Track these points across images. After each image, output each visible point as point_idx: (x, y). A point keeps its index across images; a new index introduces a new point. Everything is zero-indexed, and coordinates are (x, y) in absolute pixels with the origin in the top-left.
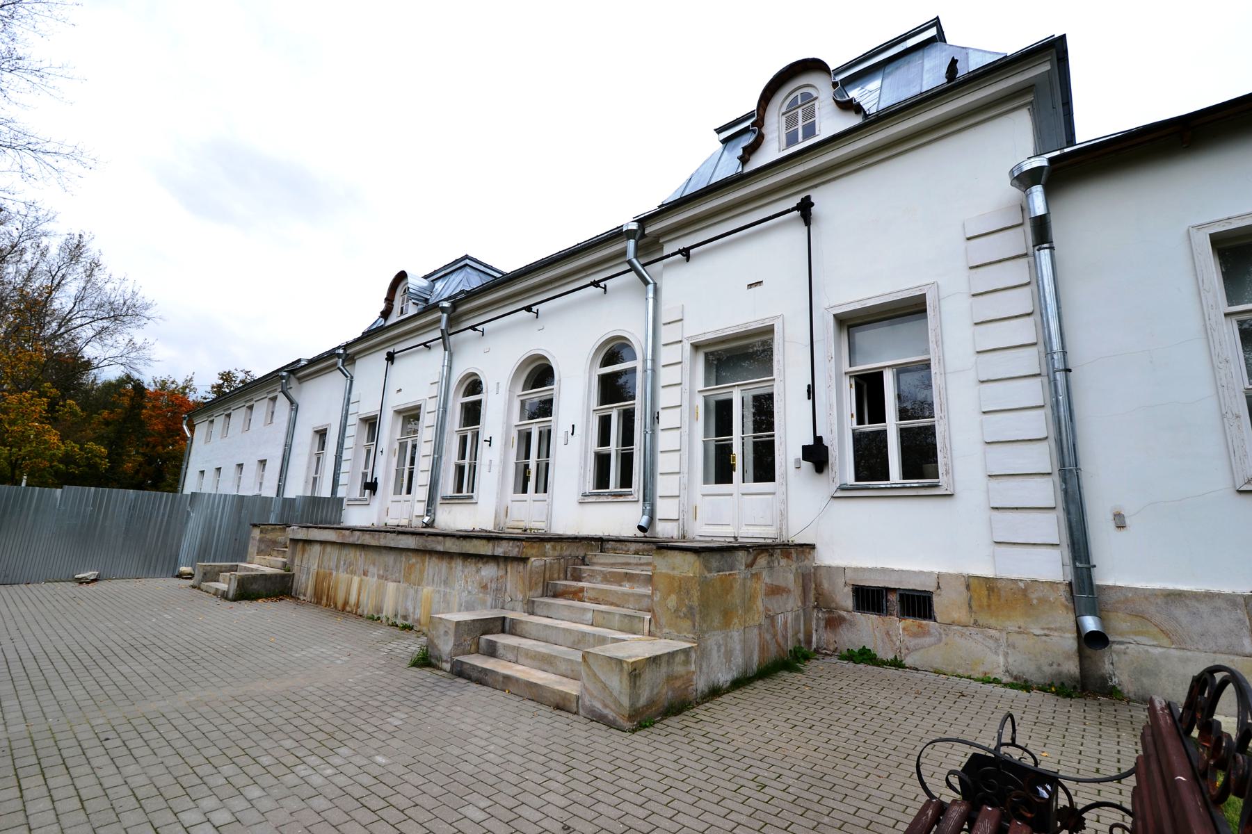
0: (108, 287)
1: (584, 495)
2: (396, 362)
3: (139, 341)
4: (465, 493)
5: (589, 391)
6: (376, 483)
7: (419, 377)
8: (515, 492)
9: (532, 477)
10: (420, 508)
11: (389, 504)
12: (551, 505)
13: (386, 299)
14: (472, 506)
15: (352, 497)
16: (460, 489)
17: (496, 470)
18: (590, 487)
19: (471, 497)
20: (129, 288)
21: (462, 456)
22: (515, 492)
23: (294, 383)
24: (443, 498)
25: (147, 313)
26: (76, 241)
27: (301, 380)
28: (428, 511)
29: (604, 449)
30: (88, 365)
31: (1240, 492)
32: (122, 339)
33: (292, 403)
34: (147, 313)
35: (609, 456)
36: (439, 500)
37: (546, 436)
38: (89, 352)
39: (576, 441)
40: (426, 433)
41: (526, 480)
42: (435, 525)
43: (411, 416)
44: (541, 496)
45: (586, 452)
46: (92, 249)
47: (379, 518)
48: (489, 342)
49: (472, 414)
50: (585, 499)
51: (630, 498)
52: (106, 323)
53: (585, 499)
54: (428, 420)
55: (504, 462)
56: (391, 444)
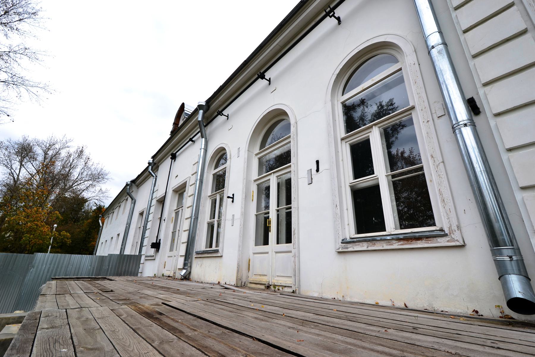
0: (93, 167)
1: (344, 242)
2: (177, 160)
3: (104, 190)
4: (214, 248)
5: (334, 120)
6: (160, 243)
7: (190, 162)
8: (256, 244)
9: (277, 227)
10: (181, 262)
11: (166, 259)
12: (297, 256)
13: (174, 124)
14: (218, 260)
15: (148, 254)
16: (211, 246)
17: (238, 223)
18: (350, 229)
19: (217, 251)
20: (99, 167)
21: (213, 216)
22: (256, 244)
23: (134, 188)
24: (197, 253)
25: (106, 177)
26: (80, 149)
27: (138, 186)
28: (185, 264)
29: (365, 182)
30: (84, 201)
31: (339, 252)
32: (98, 188)
33: (132, 199)
34: (106, 177)
35: (376, 189)
36: (194, 255)
37: (287, 187)
38: (86, 195)
39: (323, 179)
40: (188, 201)
41: (267, 230)
42: (191, 277)
43: (180, 191)
44: (284, 246)
45: (340, 187)
46: (86, 153)
47: (158, 270)
48: (232, 121)
49: (220, 181)
50: (345, 249)
51: (442, 242)
52: (91, 182)
53: (345, 249)
54: (190, 190)
55: (245, 214)
56: (170, 214)
